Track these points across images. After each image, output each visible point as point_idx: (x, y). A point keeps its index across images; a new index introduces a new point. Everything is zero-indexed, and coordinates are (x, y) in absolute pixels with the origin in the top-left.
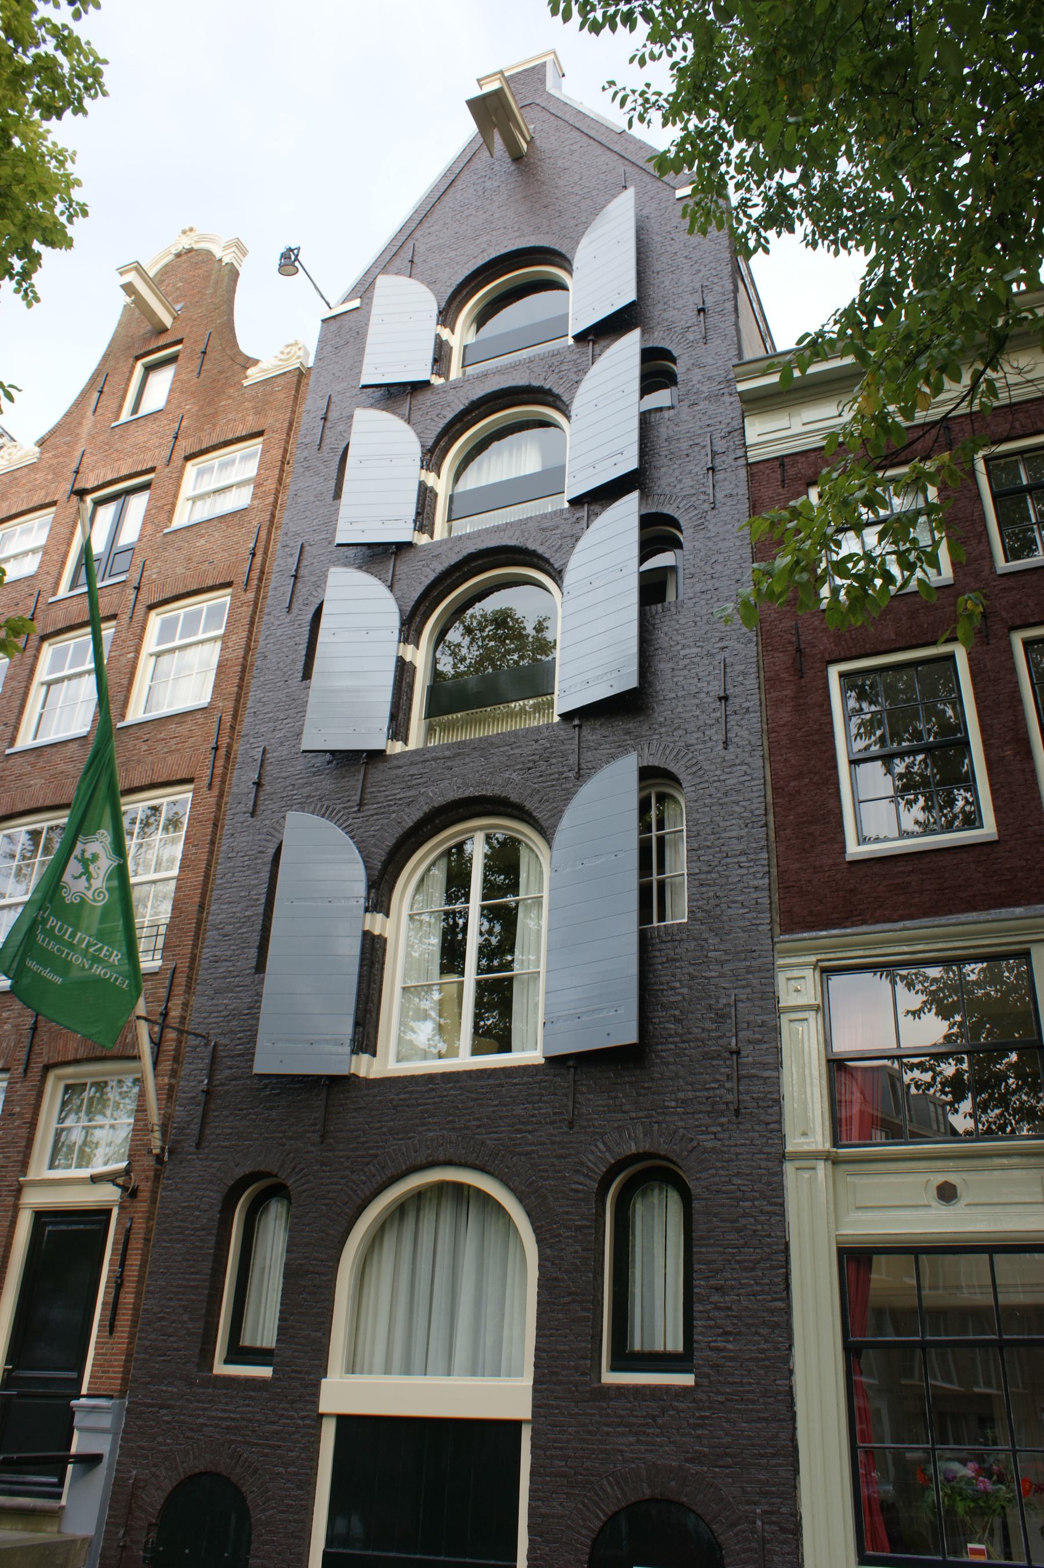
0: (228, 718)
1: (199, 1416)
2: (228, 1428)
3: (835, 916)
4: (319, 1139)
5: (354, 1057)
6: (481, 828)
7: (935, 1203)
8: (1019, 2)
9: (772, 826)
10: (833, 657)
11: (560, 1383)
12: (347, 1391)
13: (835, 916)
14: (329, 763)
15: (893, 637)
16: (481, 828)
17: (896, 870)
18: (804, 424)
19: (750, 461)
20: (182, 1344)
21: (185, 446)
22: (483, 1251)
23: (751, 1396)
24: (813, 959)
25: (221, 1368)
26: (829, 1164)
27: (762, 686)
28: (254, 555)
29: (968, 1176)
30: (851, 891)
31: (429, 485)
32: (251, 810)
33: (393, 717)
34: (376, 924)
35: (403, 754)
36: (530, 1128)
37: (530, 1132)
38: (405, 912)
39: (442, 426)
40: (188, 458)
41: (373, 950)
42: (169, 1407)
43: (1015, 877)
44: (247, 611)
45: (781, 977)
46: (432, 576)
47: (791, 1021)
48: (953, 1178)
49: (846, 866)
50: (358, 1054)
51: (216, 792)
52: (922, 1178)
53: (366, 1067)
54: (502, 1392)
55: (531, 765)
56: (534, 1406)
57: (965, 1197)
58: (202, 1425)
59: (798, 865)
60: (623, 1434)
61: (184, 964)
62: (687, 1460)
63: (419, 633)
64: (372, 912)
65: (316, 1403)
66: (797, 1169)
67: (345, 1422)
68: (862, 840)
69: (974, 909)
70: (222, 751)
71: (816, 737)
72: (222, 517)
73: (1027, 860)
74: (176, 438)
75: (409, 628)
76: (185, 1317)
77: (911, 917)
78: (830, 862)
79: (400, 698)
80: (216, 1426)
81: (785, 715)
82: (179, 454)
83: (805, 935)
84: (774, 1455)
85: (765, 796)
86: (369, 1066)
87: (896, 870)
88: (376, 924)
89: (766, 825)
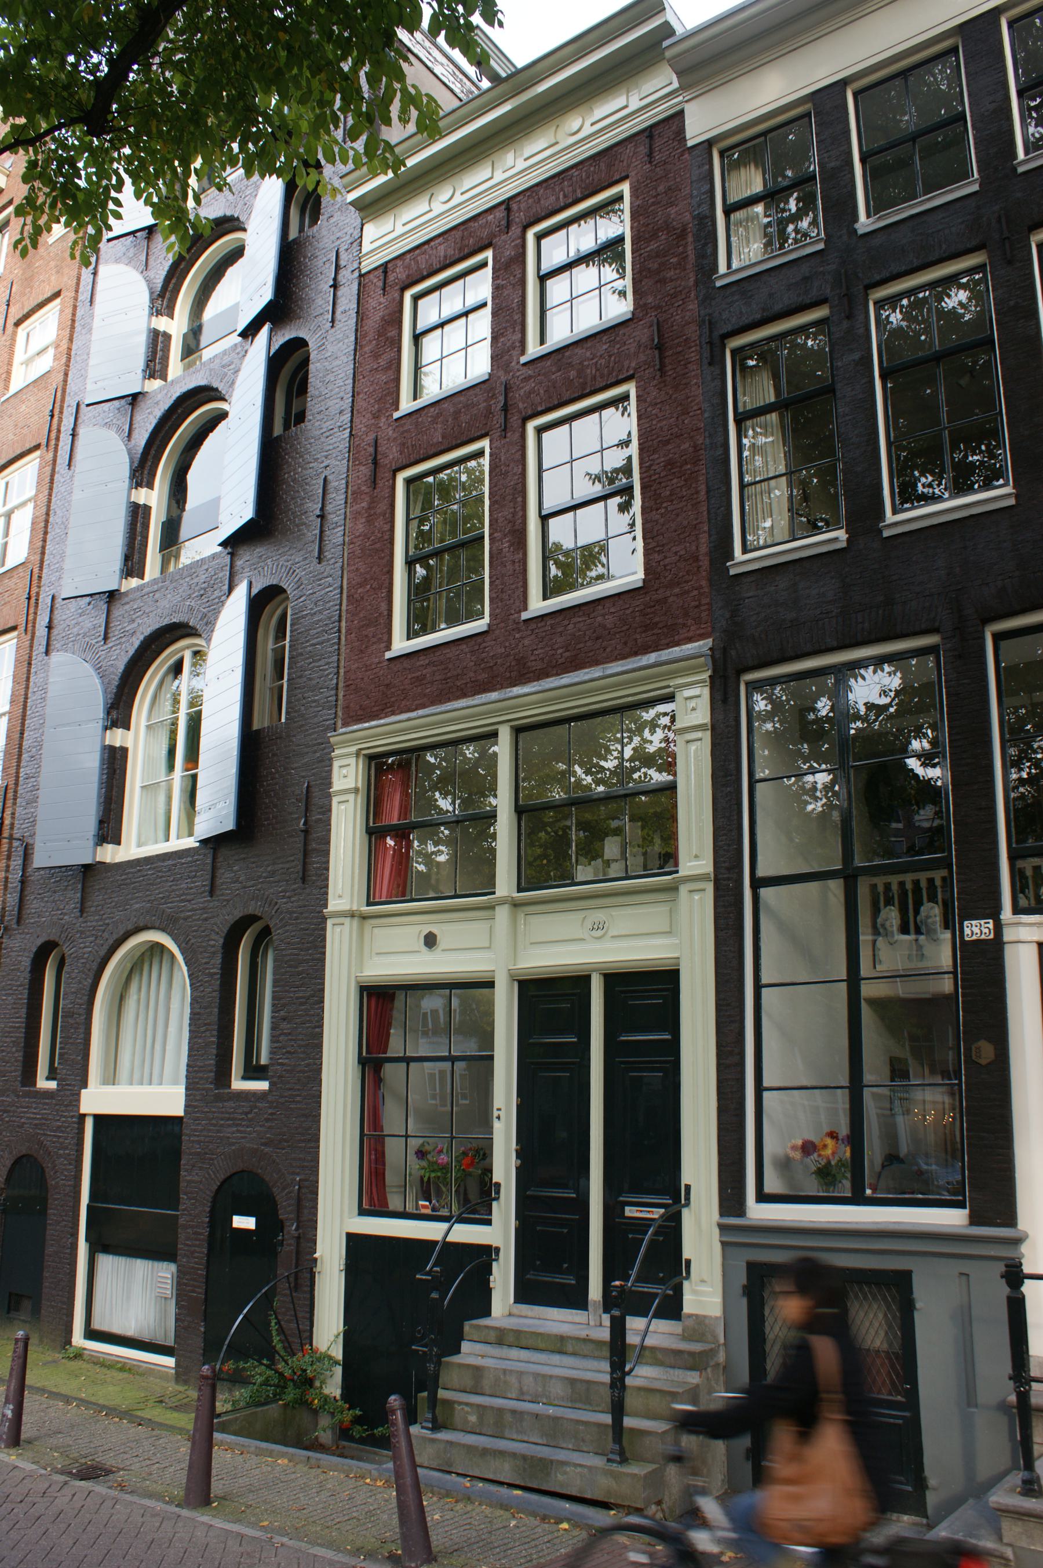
0: (36, 570)
1: (22, 1117)
2: (36, 1125)
3: (375, 709)
4: (79, 914)
5: (99, 848)
6: (188, 647)
7: (424, 949)
8: (156, 3)
9: (343, 631)
10: (398, 465)
11: (198, 1089)
12: (98, 1099)
13: (375, 709)
14: (89, 604)
15: (440, 440)
16: (188, 647)
17: (418, 664)
18: (525, 160)
19: (363, 271)
20: (13, 1068)
21: (15, 313)
22: (122, 998)
23: (298, 1098)
24: (354, 749)
25: (238, 1085)
26: (356, 921)
27: (349, 501)
28: (52, 416)
29: (446, 927)
30: (387, 685)
31: (161, 329)
32: (44, 650)
33: (127, 558)
34: (117, 737)
35: (140, 588)
36: (188, 897)
37: (189, 901)
38: (143, 723)
39: (167, 268)
40: (17, 324)
41: (115, 762)
42: (9, 1111)
43: (496, 664)
44: (49, 469)
45: (336, 764)
46: (154, 422)
47: (688, 742)
48: (435, 929)
49: (386, 663)
50: (101, 845)
51: (29, 637)
52: (416, 929)
53: (110, 854)
54: (166, 1098)
55: (202, 592)
56: (186, 1106)
57: (442, 941)
58: (24, 1123)
59: (356, 665)
60: (229, 1126)
61: (12, 782)
62: (262, 1144)
63: (153, 475)
64: (111, 728)
65: (78, 1107)
66: (690, 891)
67: (98, 1118)
68: (745, 551)
69: (464, 695)
70: (33, 601)
71: (378, 546)
72: (35, 381)
73: (505, 647)
74: (8, 305)
75: (142, 473)
76: (14, 1049)
77: (423, 706)
78: (377, 660)
79: (135, 539)
80: (31, 1124)
81: (361, 528)
82: (11, 321)
83: (355, 727)
84: (309, 1140)
85: (341, 605)
86: (113, 855)
87: (418, 664)
88: (117, 737)
89: (339, 631)
